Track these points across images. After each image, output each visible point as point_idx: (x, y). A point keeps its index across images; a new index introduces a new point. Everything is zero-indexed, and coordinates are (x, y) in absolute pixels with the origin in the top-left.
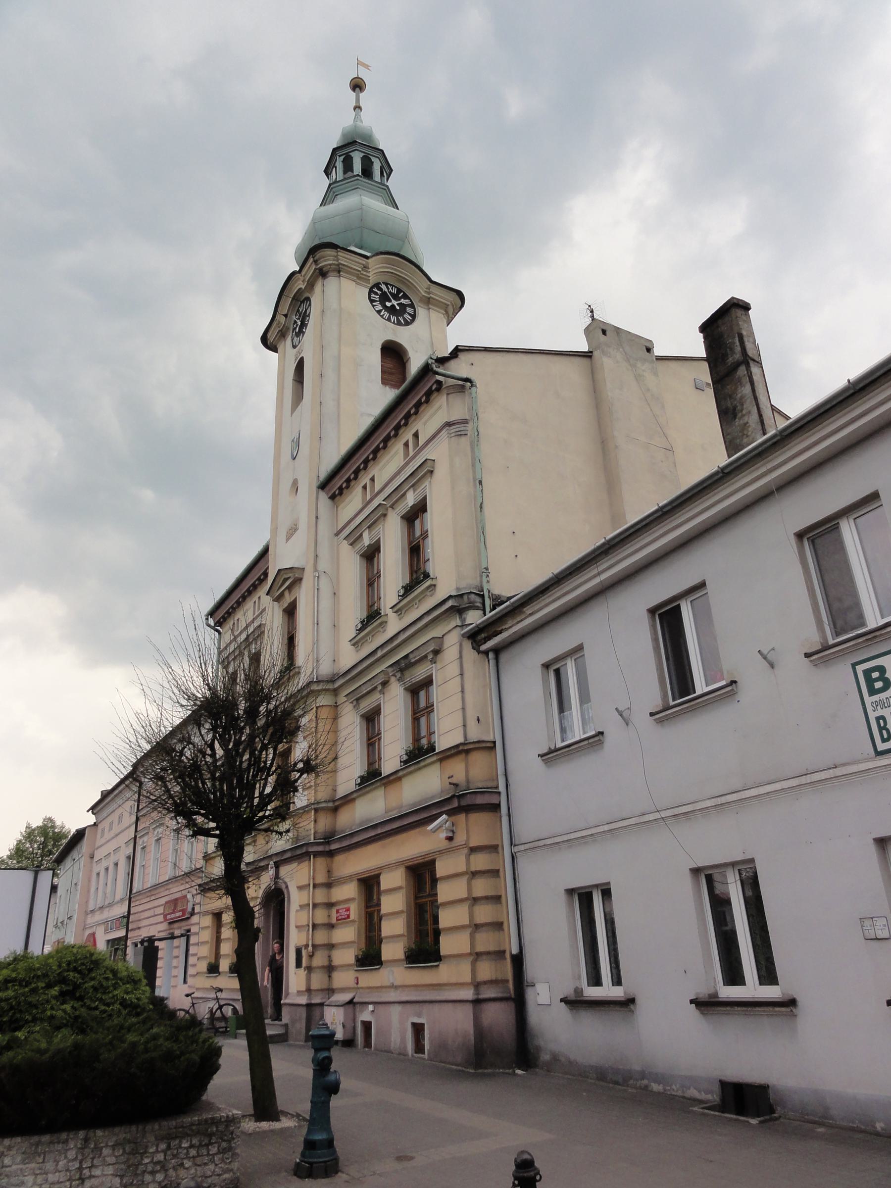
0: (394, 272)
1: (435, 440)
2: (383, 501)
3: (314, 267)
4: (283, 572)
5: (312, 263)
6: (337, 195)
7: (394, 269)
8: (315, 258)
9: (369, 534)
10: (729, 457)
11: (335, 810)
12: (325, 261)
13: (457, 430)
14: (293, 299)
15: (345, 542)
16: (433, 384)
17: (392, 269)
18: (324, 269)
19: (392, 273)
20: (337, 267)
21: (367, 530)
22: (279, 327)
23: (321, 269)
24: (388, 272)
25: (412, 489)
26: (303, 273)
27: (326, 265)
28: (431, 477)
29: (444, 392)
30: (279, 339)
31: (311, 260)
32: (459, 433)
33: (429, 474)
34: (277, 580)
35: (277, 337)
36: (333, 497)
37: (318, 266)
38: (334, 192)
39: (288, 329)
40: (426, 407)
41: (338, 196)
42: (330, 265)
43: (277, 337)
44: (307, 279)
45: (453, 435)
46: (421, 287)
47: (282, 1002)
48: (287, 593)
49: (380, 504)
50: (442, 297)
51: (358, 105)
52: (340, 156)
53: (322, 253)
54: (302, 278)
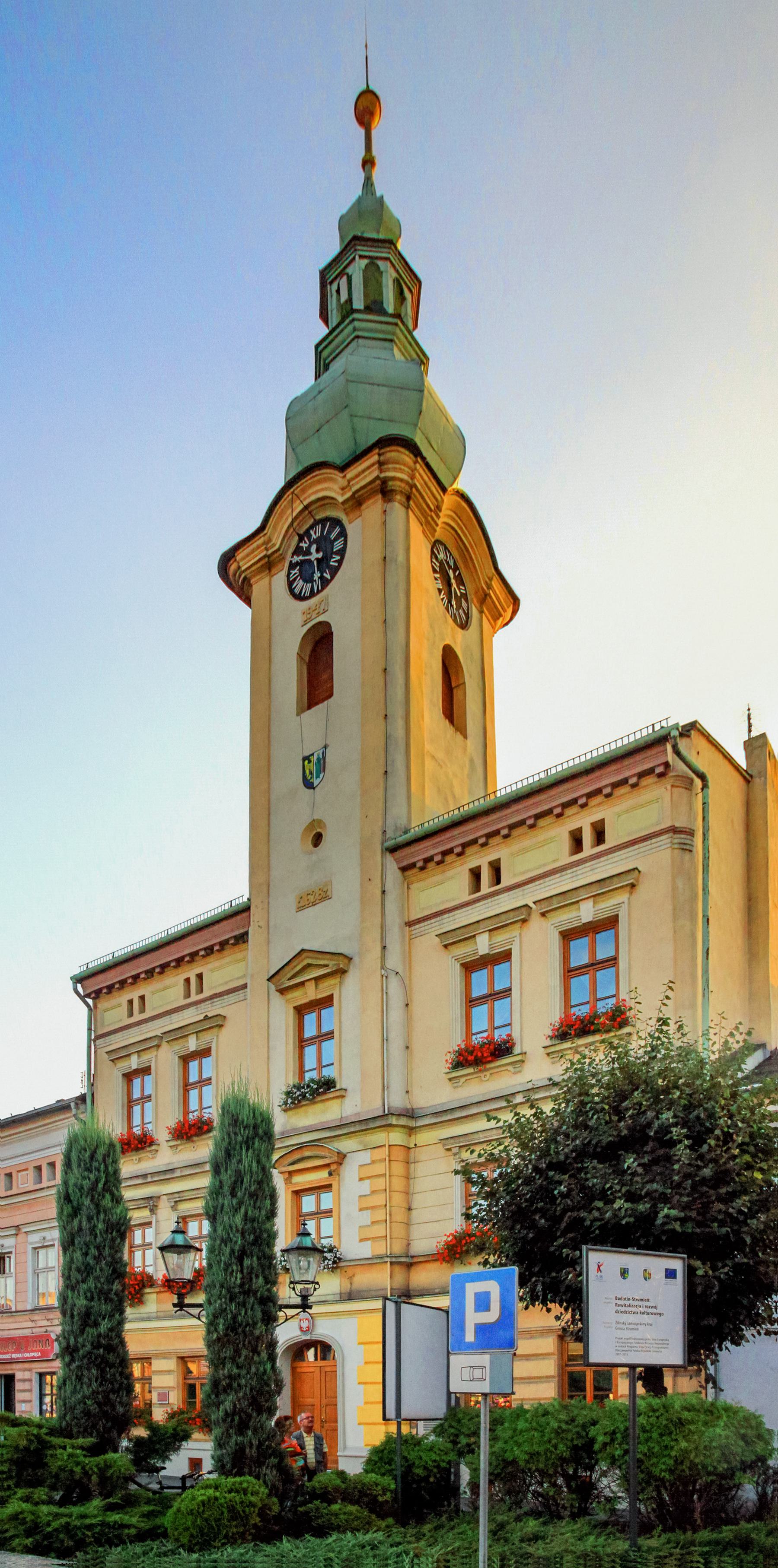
0: (459, 532)
1: (645, 843)
2: (534, 903)
3: (376, 473)
4: (305, 955)
5: (373, 465)
6: (357, 337)
7: (461, 529)
8: (382, 458)
9: (490, 940)
10: (470, 894)
11: (409, 1266)
12: (395, 469)
13: (683, 841)
14: (306, 508)
15: (437, 939)
16: (659, 765)
17: (458, 525)
18: (390, 483)
19: (456, 532)
20: (407, 488)
21: (487, 933)
22: (267, 549)
23: (385, 481)
24: (453, 528)
25: (592, 899)
26: (351, 473)
27: (394, 479)
28: (631, 893)
29: (668, 782)
30: (260, 571)
31: (374, 458)
32: (685, 847)
33: (628, 888)
34: (293, 964)
35: (259, 565)
36: (404, 869)
37: (382, 475)
38: (355, 329)
39: (282, 558)
40: (629, 793)
41: (361, 341)
42: (401, 480)
43: (259, 565)
44: (354, 489)
45: (676, 846)
46: (482, 574)
47: (339, 1454)
48: (311, 986)
49: (526, 906)
50: (498, 599)
51: (368, 157)
52: (361, 257)
53: (393, 454)
54: (343, 482)
